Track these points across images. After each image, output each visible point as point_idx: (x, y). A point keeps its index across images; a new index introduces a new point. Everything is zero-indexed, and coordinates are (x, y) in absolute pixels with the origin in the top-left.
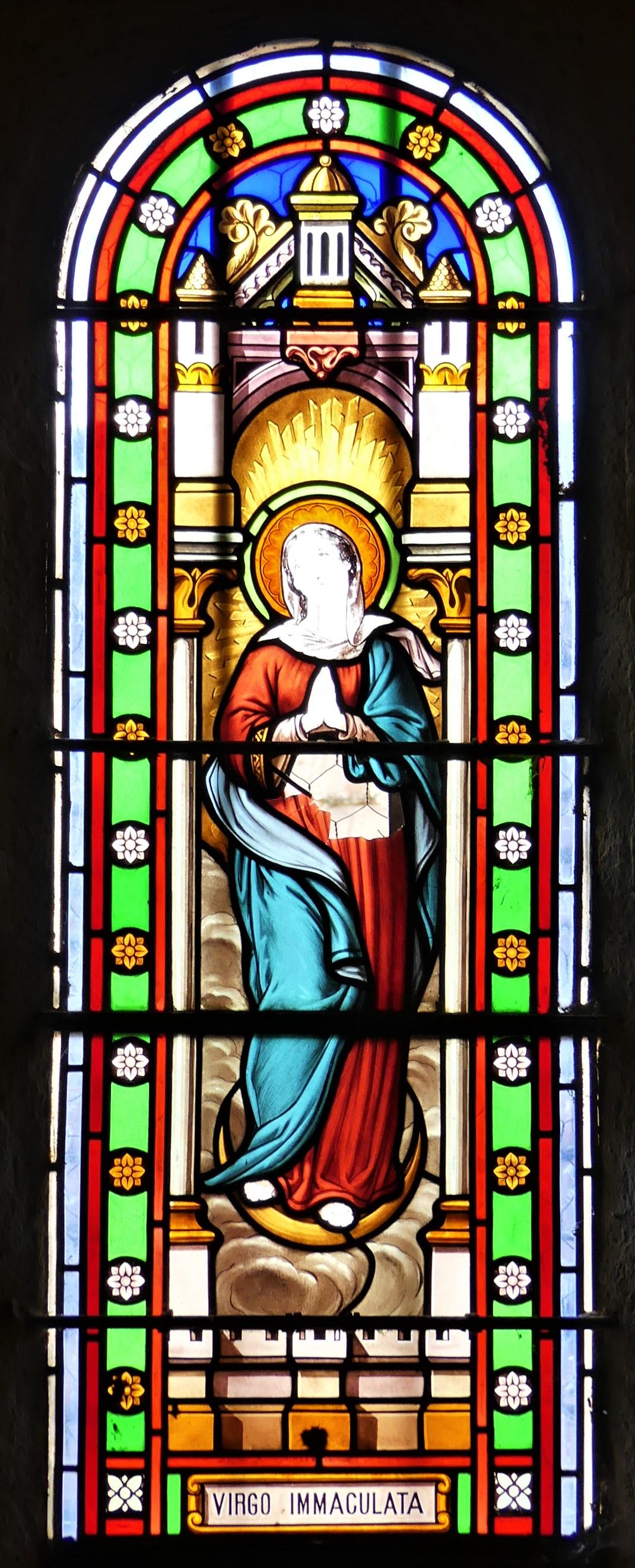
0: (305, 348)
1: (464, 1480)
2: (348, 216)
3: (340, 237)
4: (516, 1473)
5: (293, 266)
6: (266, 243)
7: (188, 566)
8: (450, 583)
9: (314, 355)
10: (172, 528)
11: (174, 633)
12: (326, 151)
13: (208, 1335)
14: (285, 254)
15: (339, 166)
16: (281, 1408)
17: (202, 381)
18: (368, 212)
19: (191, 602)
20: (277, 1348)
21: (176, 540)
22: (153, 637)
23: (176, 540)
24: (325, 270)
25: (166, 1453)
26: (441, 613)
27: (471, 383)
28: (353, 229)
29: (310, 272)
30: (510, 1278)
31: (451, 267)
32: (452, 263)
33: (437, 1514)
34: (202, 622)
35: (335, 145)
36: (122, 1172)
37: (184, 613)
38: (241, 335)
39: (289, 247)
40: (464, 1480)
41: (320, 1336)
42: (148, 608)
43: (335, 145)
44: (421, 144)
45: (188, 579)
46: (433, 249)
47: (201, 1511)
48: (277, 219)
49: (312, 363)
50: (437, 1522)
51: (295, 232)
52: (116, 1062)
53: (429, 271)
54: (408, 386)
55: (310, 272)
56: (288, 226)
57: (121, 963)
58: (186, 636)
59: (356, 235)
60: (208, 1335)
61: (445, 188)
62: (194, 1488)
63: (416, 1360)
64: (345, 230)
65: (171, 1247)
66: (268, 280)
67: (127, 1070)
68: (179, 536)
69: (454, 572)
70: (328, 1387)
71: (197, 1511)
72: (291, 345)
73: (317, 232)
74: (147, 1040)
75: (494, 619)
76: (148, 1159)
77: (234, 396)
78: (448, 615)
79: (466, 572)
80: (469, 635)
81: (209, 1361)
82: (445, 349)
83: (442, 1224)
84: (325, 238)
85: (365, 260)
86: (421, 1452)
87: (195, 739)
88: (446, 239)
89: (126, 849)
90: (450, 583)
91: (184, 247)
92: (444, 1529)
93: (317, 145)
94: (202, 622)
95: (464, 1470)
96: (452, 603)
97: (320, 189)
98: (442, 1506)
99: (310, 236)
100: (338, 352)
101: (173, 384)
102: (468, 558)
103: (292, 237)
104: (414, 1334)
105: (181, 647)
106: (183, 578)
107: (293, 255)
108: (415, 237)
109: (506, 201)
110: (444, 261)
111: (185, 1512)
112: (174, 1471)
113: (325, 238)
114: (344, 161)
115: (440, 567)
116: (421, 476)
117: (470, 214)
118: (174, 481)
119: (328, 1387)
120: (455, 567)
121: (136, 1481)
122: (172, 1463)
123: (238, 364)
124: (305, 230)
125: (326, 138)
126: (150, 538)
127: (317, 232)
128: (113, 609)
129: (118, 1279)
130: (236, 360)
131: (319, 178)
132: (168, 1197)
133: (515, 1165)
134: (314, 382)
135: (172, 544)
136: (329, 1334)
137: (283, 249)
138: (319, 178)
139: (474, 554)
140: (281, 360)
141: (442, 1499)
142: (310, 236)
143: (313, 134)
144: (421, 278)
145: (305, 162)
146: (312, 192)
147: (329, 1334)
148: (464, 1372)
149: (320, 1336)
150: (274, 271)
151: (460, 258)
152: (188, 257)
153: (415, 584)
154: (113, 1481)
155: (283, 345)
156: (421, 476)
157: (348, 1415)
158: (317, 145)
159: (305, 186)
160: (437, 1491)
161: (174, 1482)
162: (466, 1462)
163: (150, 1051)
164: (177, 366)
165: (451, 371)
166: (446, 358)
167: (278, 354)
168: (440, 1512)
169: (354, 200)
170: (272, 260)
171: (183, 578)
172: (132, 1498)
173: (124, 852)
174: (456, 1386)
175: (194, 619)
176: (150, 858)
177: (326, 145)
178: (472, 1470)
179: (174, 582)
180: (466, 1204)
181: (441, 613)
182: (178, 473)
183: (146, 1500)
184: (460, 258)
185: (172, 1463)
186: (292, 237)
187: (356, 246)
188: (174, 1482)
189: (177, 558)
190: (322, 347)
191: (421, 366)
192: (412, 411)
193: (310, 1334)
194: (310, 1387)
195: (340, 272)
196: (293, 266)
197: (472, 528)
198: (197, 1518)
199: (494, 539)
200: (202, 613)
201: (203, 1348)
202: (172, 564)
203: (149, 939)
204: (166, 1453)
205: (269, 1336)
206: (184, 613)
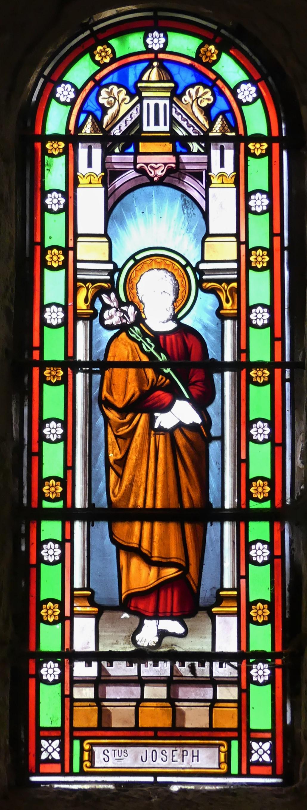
0: (147, 164)
1: (235, 744)
2: (169, 94)
3: (165, 106)
4: (262, 742)
5: (139, 120)
6: (124, 108)
7: (85, 281)
8: (226, 291)
9: (152, 167)
10: (76, 261)
11: (77, 317)
12: (156, 59)
13: (95, 664)
14: (135, 114)
15: (163, 66)
16: (134, 704)
17: (92, 182)
18: (179, 91)
19: (86, 300)
20: (132, 671)
21: (78, 267)
22: (65, 319)
23: (78, 267)
24: (157, 123)
25: (72, 729)
26: (221, 307)
27: (237, 183)
28: (172, 102)
29: (148, 125)
30: (262, 674)
31: (224, 120)
32: (225, 118)
33: (220, 764)
34: (92, 311)
35: (161, 56)
36: (53, 428)
37: (81, 304)
38: (111, 157)
39: (137, 110)
40: (235, 744)
41: (156, 665)
42: (63, 246)
43: (161, 56)
44: (259, 611)
45: (84, 288)
46: (214, 112)
47: (90, 760)
48: (132, 96)
49: (151, 172)
50: (220, 768)
51: (140, 101)
52: (43, 553)
53: (212, 123)
54: (202, 183)
55: (148, 125)
56: (137, 98)
57: (48, 496)
58: (84, 319)
59: (173, 105)
60: (95, 664)
61: (219, 77)
62: (87, 747)
63: (209, 679)
64: (167, 102)
65: (75, 616)
66: (126, 128)
67: (56, 311)
68: (79, 266)
69: (228, 285)
70: (161, 692)
71: (88, 760)
72: (139, 163)
73: (152, 103)
74: (60, 660)
75: (249, 309)
76: (63, 482)
77: (109, 190)
78: (224, 308)
79: (235, 285)
80: (236, 318)
81: (94, 679)
82: (222, 165)
83: (221, 603)
84: (157, 106)
85: (179, 118)
86: (211, 728)
87: (88, 360)
88: (222, 104)
89: (57, 199)
90: (226, 291)
91: (81, 111)
92: (224, 772)
93: (152, 56)
94: (92, 311)
95: (234, 738)
96: (227, 301)
97: (153, 80)
98: (222, 759)
99: (148, 105)
100: (165, 167)
101: (76, 183)
102: (235, 276)
103: (139, 105)
104: (207, 664)
105: (80, 325)
106: (81, 287)
107: (138, 114)
108: (204, 104)
109: (253, 85)
110: (221, 117)
111: (82, 761)
112: (77, 738)
113: (157, 106)
114: (168, 65)
115: (220, 281)
116: (210, 233)
117: (234, 92)
118: (76, 235)
119: (161, 692)
120: (229, 282)
121: (56, 743)
122: (76, 734)
123: (110, 171)
124: (145, 102)
125: (156, 53)
126: (64, 266)
127: (152, 103)
128: (44, 303)
129: (47, 670)
130: (108, 170)
131: (154, 74)
132: (72, 589)
133: (211, 57)
134: (152, 182)
135: (76, 270)
136: (161, 663)
137: (134, 111)
138: (154, 74)
139: (239, 274)
140: (134, 170)
141: (222, 755)
142: (148, 105)
143: (149, 51)
144: (208, 127)
145: (145, 64)
146: (148, 81)
147: (161, 663)
148: (234, 685)
149: (156, 665)
150: (129, 123)
151: (229, 115)
152: (83, 117)
153: (206, 291)
154: (44, 743)
155: (135, 163)
156: (210, 233)
157: (171, 709)
158: (152, 56)
159: (145, 78)
160: (219, 751)
161: (76, 744)
162: (236, 734)
163: (62, 667)
164: (78, 174)
165: (225, 176)
166: (222, 170)
167: (132, 167)
168: (222, 763)
169: (172, 85)
170: (128, 117)
171: (81, 287)
172: (54, 752)
173: (61, 94)
174: (231, 693)
175: (87, 309)
176: (64, 438)
177: (156, 56)
178: (239, 739)
179: (76, 290)
180: (235, 593)
181: (221, 307)
182: (80, 231)
183: (62, 753)
184: (229, 115)
185: (76, 734)
186: (139, 105)
187: (174, 110)
188: (76, 744)
189: (79, 277)
190: (156, 164)
191: (210, 174)
192: (205, 197)
193: (150, 663)
194: (150, 692)
195: (165, 124)
196: (139, 120)
197: (238, 261)
198: (88, 764)
199: (249, 266)
200: (92, 306)
201: (92, 671)
202: (76, 280)
203: (63, 482)
204: (72, 729)
205: (129, 665)
206: (81, 304)
